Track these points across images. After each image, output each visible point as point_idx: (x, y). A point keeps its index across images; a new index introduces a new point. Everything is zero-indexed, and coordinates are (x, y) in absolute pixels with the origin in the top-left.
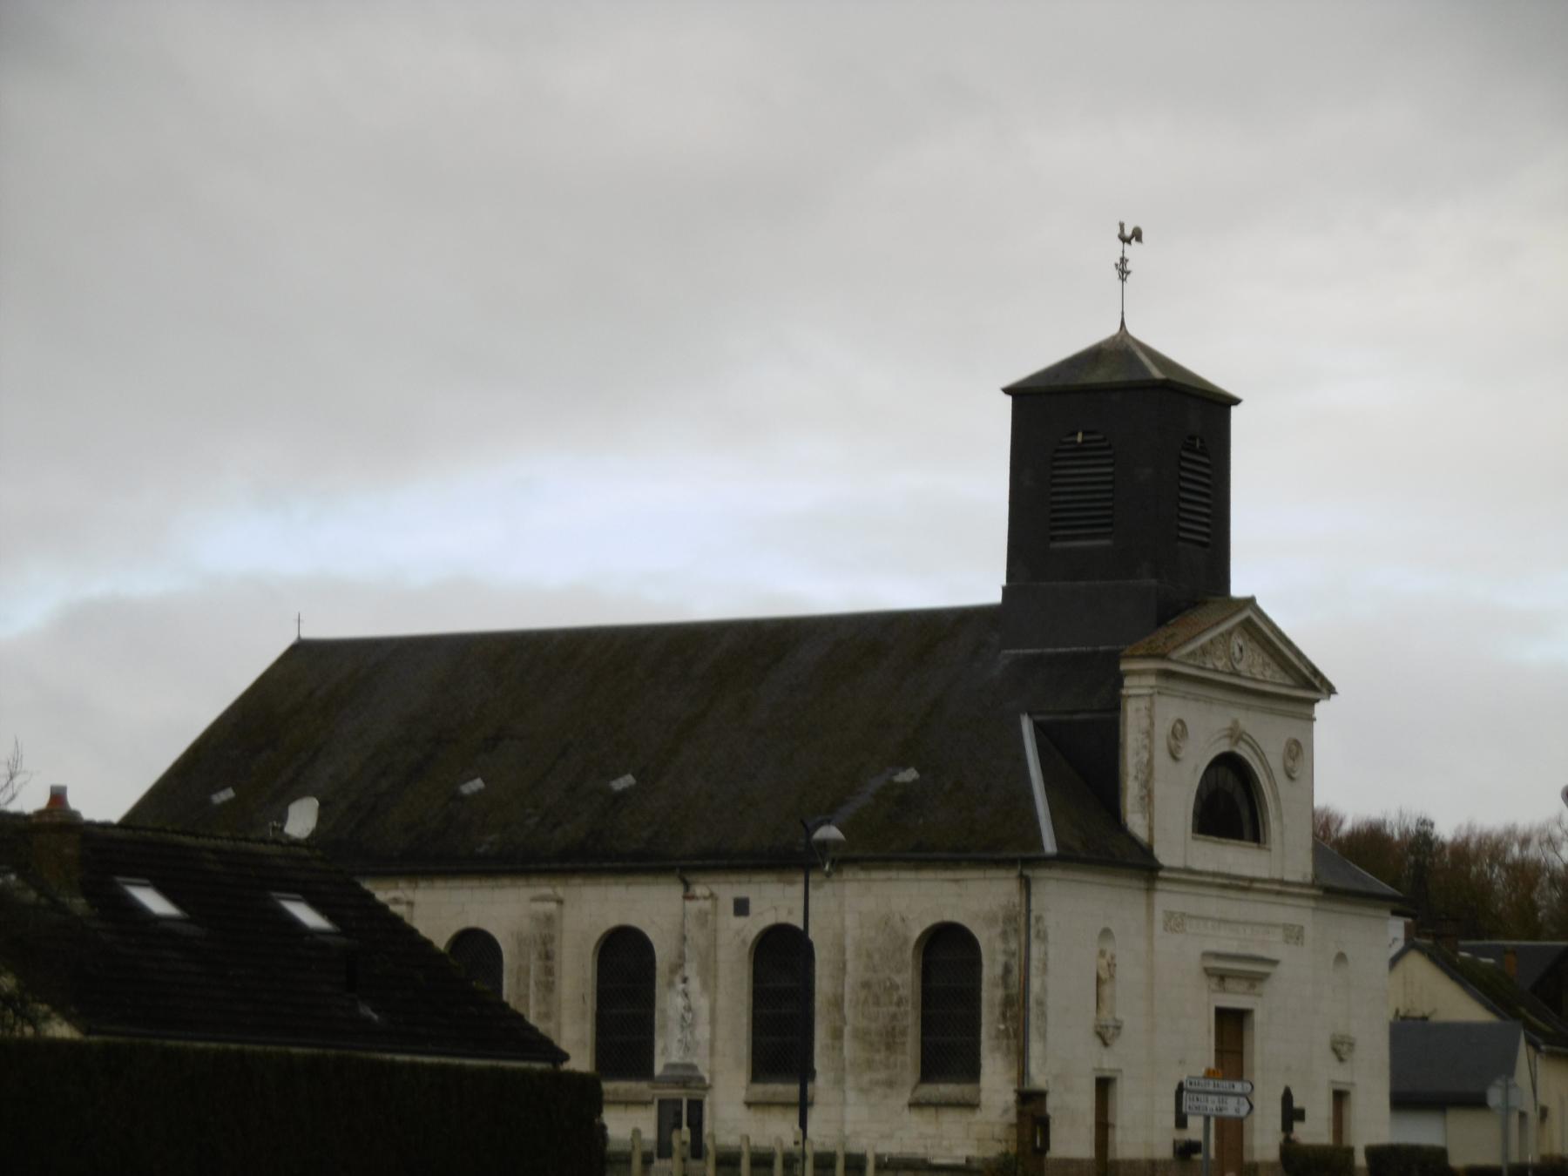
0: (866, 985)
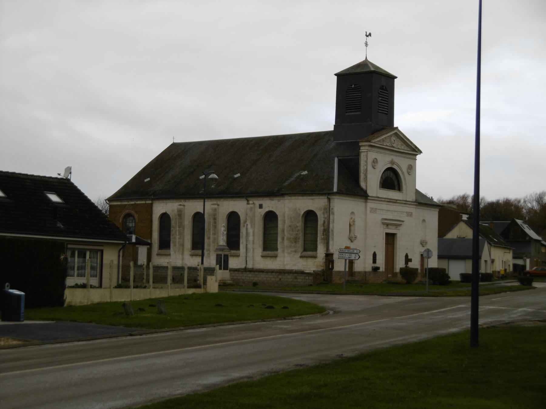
0: (290, 226)
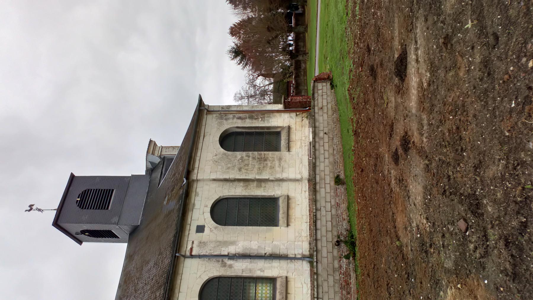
0: (240, 169)
